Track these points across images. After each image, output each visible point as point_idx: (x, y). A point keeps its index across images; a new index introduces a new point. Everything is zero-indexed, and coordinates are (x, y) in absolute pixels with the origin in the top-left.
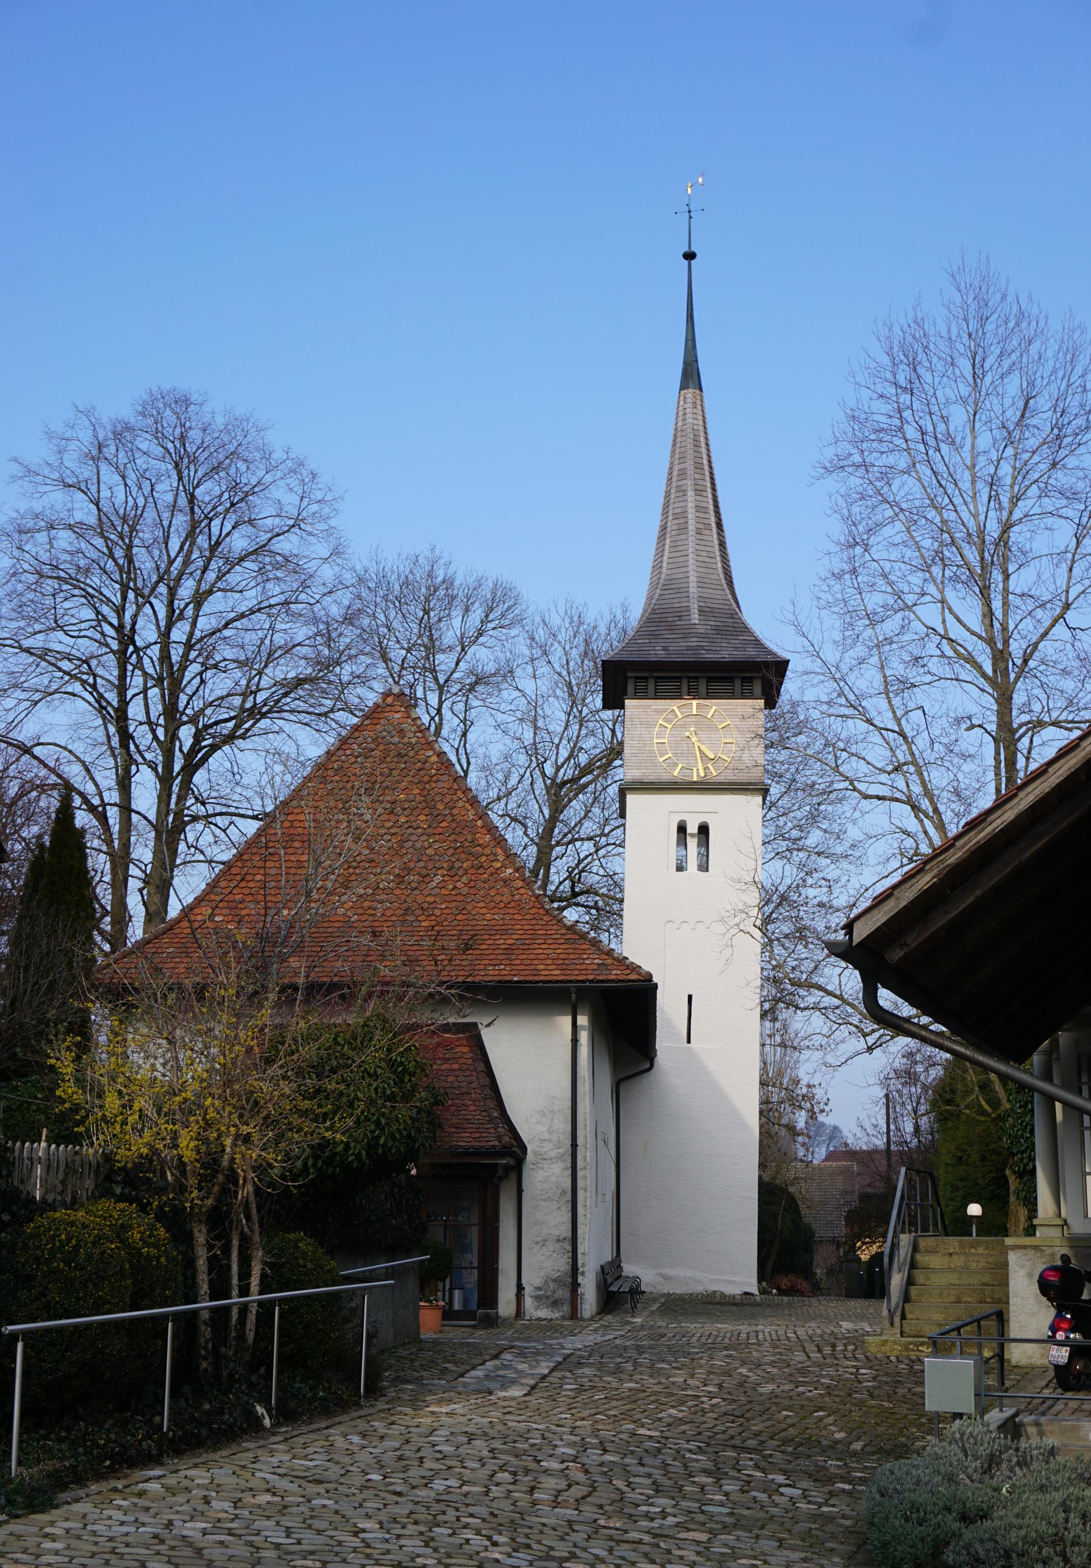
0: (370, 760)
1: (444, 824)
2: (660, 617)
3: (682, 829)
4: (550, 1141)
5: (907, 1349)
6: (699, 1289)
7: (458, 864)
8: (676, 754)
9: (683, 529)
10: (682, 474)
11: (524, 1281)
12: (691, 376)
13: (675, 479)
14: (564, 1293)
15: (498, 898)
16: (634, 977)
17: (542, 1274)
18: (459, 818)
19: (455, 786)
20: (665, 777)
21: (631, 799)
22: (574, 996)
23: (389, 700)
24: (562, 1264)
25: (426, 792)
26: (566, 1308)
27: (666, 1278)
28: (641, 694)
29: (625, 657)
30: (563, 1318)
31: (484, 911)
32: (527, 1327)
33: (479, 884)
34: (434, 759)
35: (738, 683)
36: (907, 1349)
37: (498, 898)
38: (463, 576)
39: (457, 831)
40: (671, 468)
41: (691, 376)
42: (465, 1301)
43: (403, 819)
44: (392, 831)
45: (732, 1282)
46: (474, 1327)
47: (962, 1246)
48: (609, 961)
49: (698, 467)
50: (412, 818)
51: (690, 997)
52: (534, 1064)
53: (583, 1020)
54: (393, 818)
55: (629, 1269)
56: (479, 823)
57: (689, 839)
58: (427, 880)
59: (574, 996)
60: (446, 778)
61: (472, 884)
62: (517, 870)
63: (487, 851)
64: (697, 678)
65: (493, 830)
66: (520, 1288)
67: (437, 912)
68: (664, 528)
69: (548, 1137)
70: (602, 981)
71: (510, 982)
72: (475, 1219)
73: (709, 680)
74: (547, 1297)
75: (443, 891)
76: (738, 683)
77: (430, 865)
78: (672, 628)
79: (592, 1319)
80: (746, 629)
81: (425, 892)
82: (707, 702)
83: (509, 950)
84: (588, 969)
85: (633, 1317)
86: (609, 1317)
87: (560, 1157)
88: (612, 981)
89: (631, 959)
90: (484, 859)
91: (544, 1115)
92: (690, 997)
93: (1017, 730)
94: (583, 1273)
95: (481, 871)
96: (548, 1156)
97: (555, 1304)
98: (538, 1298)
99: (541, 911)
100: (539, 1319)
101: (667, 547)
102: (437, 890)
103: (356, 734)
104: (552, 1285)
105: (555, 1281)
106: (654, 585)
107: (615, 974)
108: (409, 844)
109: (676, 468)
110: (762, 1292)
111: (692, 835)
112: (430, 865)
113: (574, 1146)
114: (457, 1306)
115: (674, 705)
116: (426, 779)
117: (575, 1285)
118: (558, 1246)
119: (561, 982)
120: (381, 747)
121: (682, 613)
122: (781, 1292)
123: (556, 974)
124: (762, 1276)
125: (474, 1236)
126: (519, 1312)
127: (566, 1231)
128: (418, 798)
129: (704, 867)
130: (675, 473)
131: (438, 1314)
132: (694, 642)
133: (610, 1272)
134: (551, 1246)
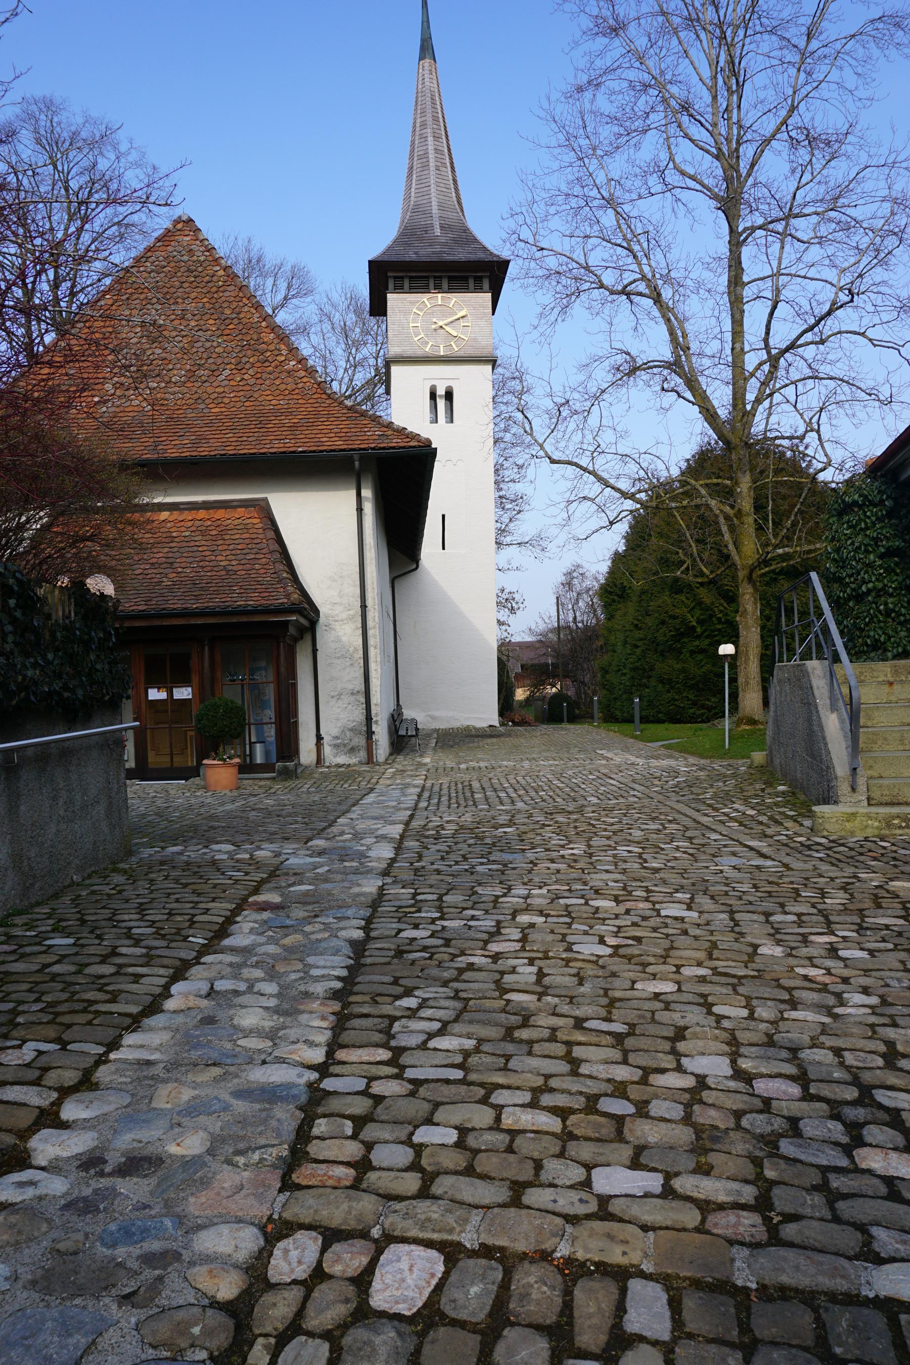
0: (162, 275)
1: (231, 327)
2: (410, 233)
3: (433, 396)
4: (341, 604)
5: (889, 825)
6: (456, 724)
7: (244, 360)
8: (426, 335)
9: (425, 166)
10: (424, 125)
11: (322, 732)
12: (426, 49)
13: (418, 129)
14: (361, 741)
15: (283, 387)
16: (413, 444)
17: (339, 725)
18: (244, 321)
19: (241, 294)
20: (419, 353)
21: (395, 370)
22: (357, 464)
23: (179, 226)
24: (358, 715)
25: (214, 301)
26: (363, 754)
27: (433, 718)
28: (399, 289)
29: (386, 258)
30: (361, 763)
31: (270, 398)
32: (325, 776)
33: (265, 376)
34: (221, 273)
35: (471, 283)
36: (889, 825)
37: (283, 387)
38: (271, 258)
39: (244, 331)
40: (415, 123)
41: (426, 49)
42: (267, 753)
43: (193, 323)
44: (184, 333)
45: (481, 718)
46: (274, 778)
47: (896, 672)
48: (390, 433)
49: (435, 119)
50: (202, 322)
51: (443, 516)
52: (322, 533)
53: (367, 493)
54: (184, 323)
55: (408, 713)
56: (264, 324)
57: (438, 400)
58: (216, 373)
59: (357, 464)
60: (232, 288)
61: (259, 375)
62: (299, 362)
63: (272, 347)
64: (440, 277)
65: (276, 329)
66: (319, 738)
67: (226, 400)
68: (411, 168)
69: (338, 600)
70: (384, 448)
71: (294, 452)
72: (271, 679)
73: (450, 279)
74: (345, 745)
75: (232, 383)
76: (471, 283)
77: (219, 361)
78: (420, 239)
79: (386, 762)
80: (475, 240)
81: (214, 384)
82: (449, 295)
83: (294, 427)
84: (370, 438)
85: (421, 756)
86: (400, 758)
87: (351, 618)
88: (393, 448)
89: (410, 429)
90: (268, 354)
91: (334, 581)
92: (443, 516)
93: (741, 234)
94: (376, 722)
95: (267, 364)
96: (340, 618)
97: (352, 750)
98: (336, 746)
99: (324, 396)
100: (339, 766)
101: (414, 185)
102: (226, 382)
103: (149, 254)
104: (348, 734)
105: (351, 730)
106: (405, 212)
107: (396, 442)
108: (200, 344)
109: (418, 121)
110: (502, 724)
111: (441, 396)
112: (219, 361)
113: (364, 607)
114: (259, 759)
115: (424, 298)
116: (214, 289)
117: (370, 733)
118: (352, 698)
119: (344, 450)
120: (172, 264)
121: (428, 228)
122: (515, 724)
123: (340, 444)
124: (501, 714)
125: (270, 693)
126: (319, 760)
127: (360, 685)
128: (207, 305)
129: (450, 419)
130: (418, 125)
131: (234, 770)
132: (438, 249)
133: (396, 718)
134: (346, 699)
